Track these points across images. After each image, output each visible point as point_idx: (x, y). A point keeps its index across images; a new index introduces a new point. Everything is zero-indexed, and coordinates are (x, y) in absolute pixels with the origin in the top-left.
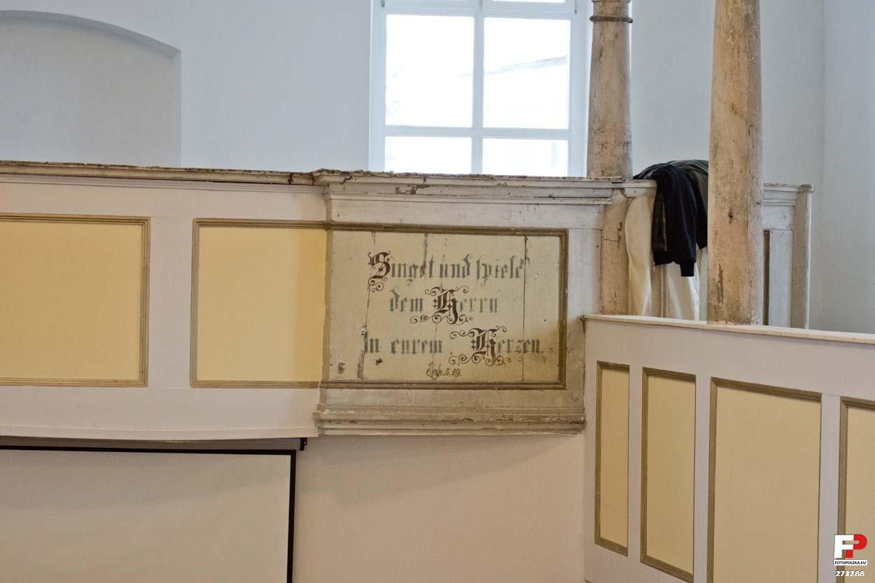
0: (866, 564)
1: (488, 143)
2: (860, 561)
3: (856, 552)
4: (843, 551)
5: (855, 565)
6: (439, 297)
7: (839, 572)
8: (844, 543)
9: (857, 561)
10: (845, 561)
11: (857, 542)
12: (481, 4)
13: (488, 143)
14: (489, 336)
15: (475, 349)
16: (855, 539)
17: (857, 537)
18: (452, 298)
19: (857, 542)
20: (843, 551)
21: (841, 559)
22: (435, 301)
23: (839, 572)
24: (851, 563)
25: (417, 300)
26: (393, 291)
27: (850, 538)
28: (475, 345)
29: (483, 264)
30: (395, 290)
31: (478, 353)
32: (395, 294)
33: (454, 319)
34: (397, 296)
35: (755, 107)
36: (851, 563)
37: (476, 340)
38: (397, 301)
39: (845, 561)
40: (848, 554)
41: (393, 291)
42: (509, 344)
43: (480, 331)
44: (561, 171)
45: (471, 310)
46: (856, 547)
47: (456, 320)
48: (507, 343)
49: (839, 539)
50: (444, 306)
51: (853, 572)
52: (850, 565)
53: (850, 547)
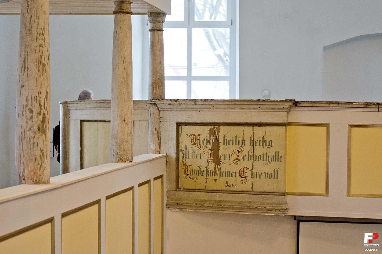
0: (378, 246)
1: (194, 83)
2: (375, 244)
3: (374, 241)
4: (368, 240)
5: (374, 246)
6: (193, 138)
7: (366, 249)
8: (369, 236)
9: (374, 244)
10: (369, 244)
11: (374, 236)
13: (194, 83)
15: (192, 142)
16: (373, 235)
17: (374, 234)
18: (199, 138)
19: (374, 236)
20: (368, 240)
21: (366, 243)
23: (366, 249)
24: (371, 245)
25: (211, 171)
26: (199, 167)
27: (371, 234)
28: (192, 141)
31: (193, 144)
34: (200, 169)
36: (371, 245)
39: (369, 244)
40: (370, 241)
41: (199, 167)
42: (235, 174)
43: (194, 135)
44: (226, 96)
46: (374, 238)
47: (200, 148)
48: (234, 173)
49: (366, 235)
51: (372, 249)
52: (371, 246)
53: (371, 238)
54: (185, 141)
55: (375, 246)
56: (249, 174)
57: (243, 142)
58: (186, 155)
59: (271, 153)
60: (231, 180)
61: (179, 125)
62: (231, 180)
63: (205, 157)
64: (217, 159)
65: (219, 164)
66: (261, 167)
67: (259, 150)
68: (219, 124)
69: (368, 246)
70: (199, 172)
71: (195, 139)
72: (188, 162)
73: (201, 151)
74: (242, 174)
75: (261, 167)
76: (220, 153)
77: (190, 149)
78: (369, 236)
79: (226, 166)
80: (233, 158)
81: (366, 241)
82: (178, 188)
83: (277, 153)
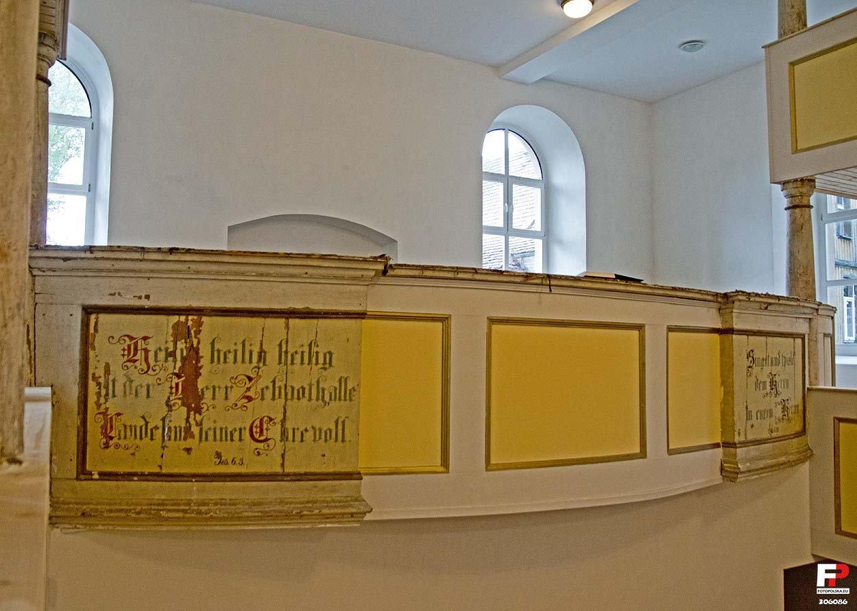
0: (848, 593)
6: (129, 346)
8: (827, 571)
12: (5, 583)
14: (141, 345)
18: (144, 346)
22: (124, 350)
28: (126, 352)
29: (825, 335)
30: (145, 416)
32: (145, 420)
33: (146, 369)
34: (147, 423)
35: (43, 210)
37: (126, 348)
38: (146, 429)
42: (214, 393)
43: (131, 338)
45: (214, 398)
50: (135, 355)
53: (833, 576)
54: (106, 353)
55: (841, 593)
56: (274, 432)
57: (262, 355)
58: (107, 390)
59: (330, 384)
60: (229, 450)
61: (88, 310)
62: (229, 450)
63: (161, 394)
64: (192, 399)
65: (198, 410)
66: (302, 415)
67: (300, 376)
68: (200, 312)
69: (825, 593)
70: (146, 431)
71: (133, 349)
72: (112, 406)
73: (149, 379)
74: (257, 432)
75: (302, 415)
76: (201, 384)
77: (118, 373)
78: (827, 571)
79: (213, 416)
80: (236, 393)
81: (820, 582)
82: (83, 472)
83: (343, 381)
